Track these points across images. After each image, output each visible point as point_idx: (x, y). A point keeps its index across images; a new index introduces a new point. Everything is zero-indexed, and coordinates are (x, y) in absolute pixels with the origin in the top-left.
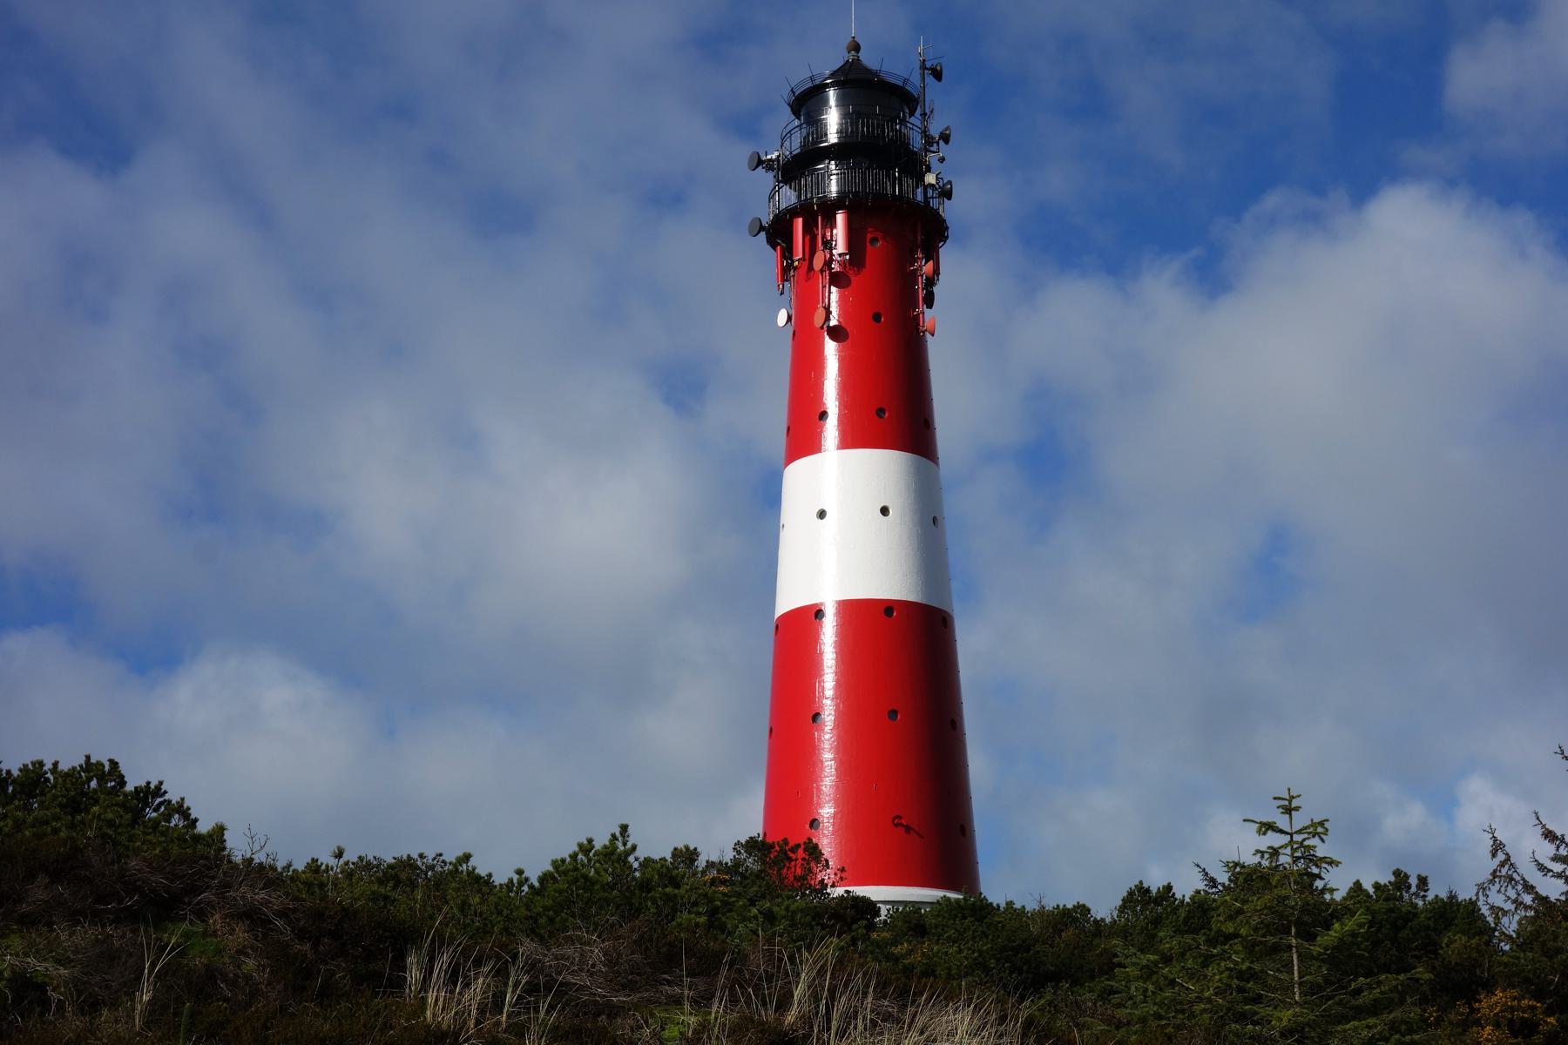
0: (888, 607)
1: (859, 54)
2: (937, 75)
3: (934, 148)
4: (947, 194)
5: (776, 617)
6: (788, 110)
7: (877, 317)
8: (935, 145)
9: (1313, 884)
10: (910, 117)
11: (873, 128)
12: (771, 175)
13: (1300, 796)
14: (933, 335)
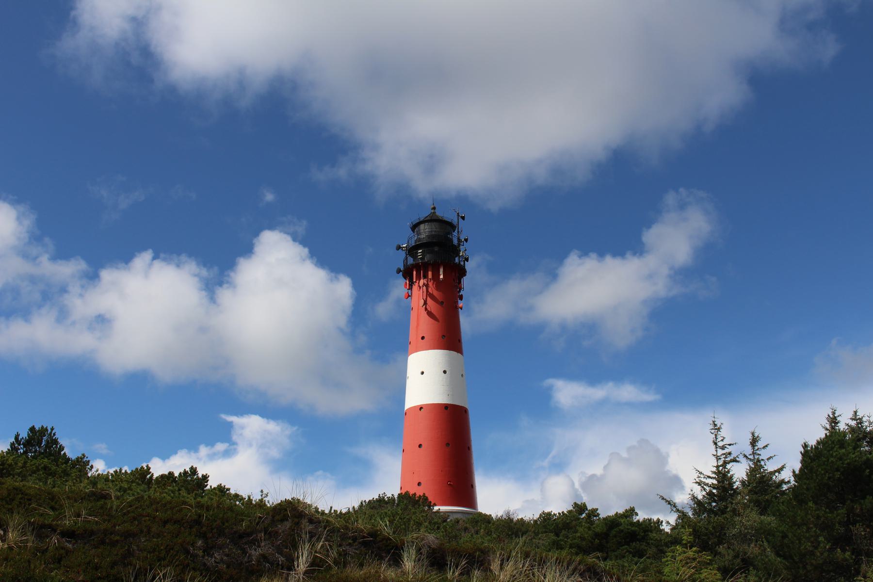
2: (463, 218)
3: (462, 244)
4: (467, 260)
5: (405, 409)
6: (410, 230)
7: (445, 372)
9: (18, 438)
14: (467, 242)
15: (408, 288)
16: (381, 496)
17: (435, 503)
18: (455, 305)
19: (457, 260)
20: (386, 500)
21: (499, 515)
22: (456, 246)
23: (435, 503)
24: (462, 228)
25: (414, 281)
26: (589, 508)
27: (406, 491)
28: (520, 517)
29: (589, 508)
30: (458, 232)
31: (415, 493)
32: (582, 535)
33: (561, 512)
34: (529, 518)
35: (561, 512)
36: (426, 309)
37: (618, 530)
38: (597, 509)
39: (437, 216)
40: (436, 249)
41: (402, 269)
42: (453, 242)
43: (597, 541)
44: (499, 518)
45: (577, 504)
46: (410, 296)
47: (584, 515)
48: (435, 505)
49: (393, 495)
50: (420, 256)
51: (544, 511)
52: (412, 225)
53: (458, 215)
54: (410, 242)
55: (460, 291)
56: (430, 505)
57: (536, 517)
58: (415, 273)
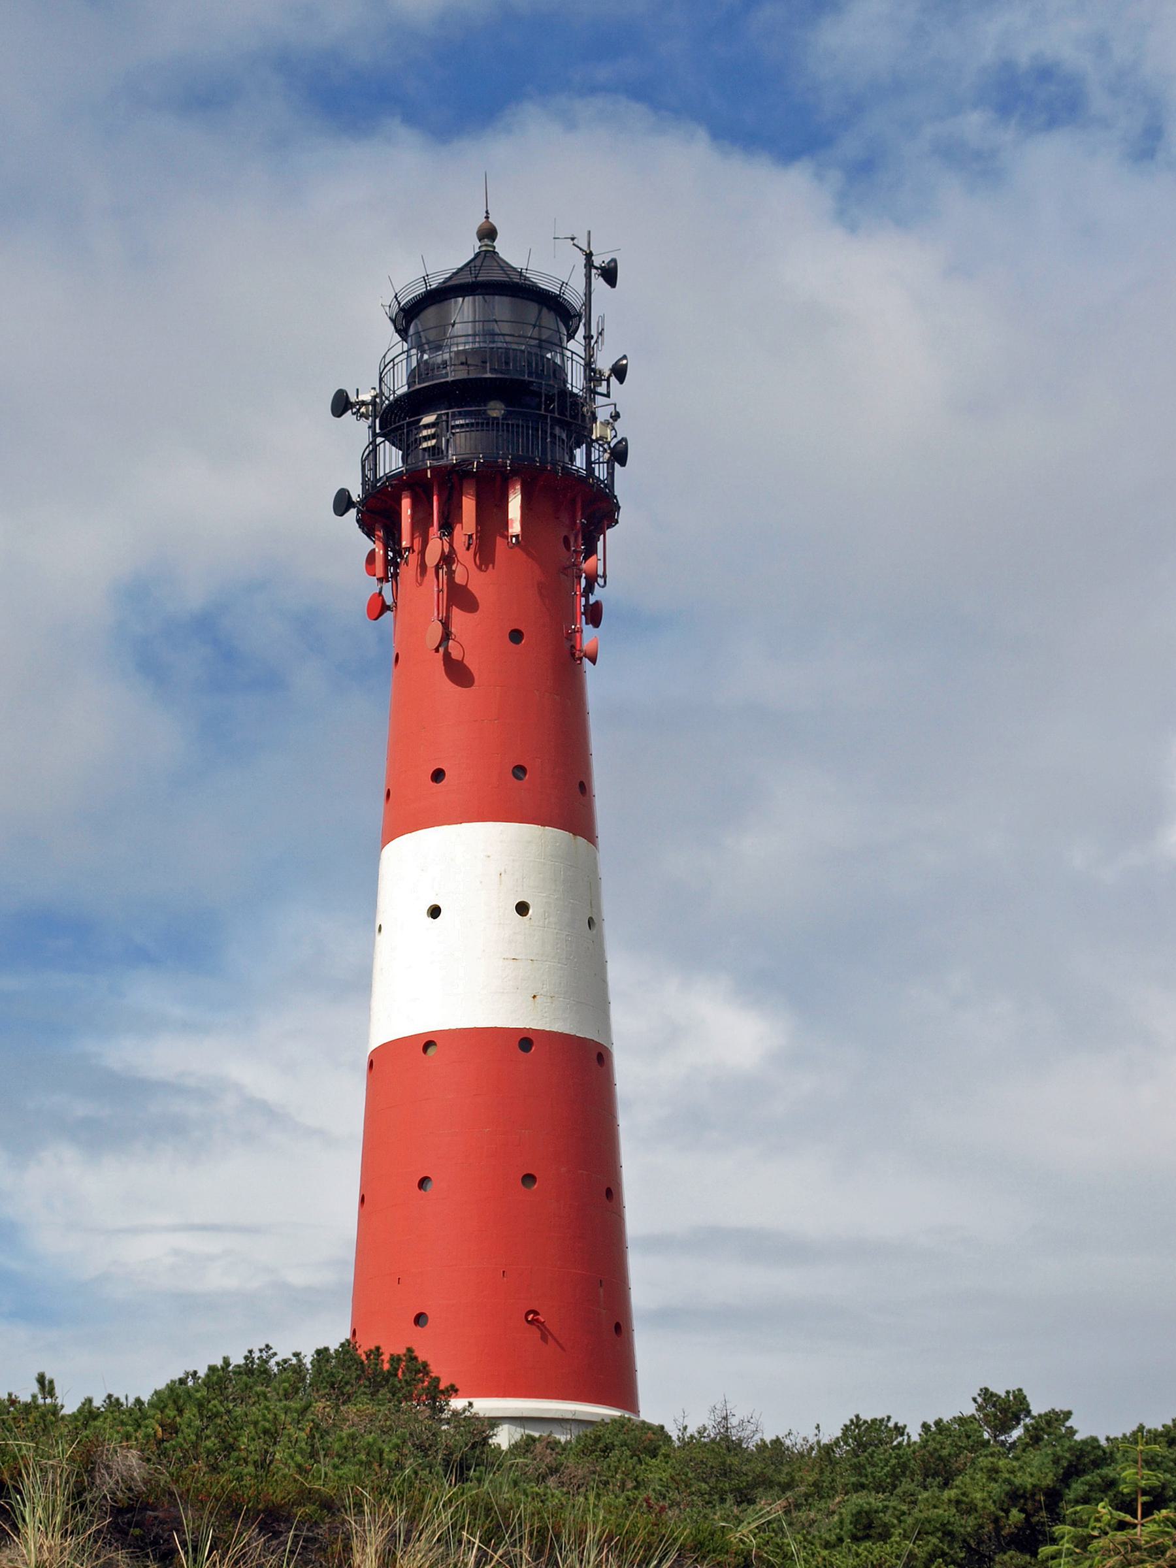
0: (526, 1040)
1: (495, 244)
3: (602, 389)
7: (522, 908)
8: (604, 383)
10: (568, 341)
11: (523, 433)
12: (365, 424)
13: (683, 1410)
15: (380, 572)
16: (256, 1355)
17: (452, 1386)
18: (567, 645)
19: (580, 461)
20: (276, 1369)
21: (692, 1430)
22: (576, 395)
23: (452, 1386)
24: (603, 318)
25: (404, 544)
26: (1038, 1408)
27: (937, 1419)
28: (769, 1438)
29: (1038, 1408)
30: (588, 337)
31: (378, 1349)
32: (964, 1494)
33: (931, 1422)
34: (804, 1439)
35: (931, 1422)
36: (447, 656)
37: (1099, 1480)
38: (1068, 1415)
39: (505, 266)
40: (496, 410)
41: (356, 493)
42: (565, 382)
43: (1016, 1515)
44: (692, 1437)
45: (992, 1395)
46: (388, 608)
47: (1017, 1433)
48: (453, 1391)
49: (296, 1355)
50: (427, 438)
51: (857, 1417)
52: (395, 309)
53: (589, 264)
54: (388, 379)
55: (589, 589)
56: (437, 1394)
57: (831, 1432)
58: (406, 505)
